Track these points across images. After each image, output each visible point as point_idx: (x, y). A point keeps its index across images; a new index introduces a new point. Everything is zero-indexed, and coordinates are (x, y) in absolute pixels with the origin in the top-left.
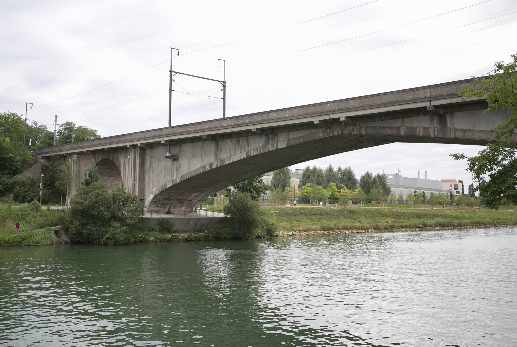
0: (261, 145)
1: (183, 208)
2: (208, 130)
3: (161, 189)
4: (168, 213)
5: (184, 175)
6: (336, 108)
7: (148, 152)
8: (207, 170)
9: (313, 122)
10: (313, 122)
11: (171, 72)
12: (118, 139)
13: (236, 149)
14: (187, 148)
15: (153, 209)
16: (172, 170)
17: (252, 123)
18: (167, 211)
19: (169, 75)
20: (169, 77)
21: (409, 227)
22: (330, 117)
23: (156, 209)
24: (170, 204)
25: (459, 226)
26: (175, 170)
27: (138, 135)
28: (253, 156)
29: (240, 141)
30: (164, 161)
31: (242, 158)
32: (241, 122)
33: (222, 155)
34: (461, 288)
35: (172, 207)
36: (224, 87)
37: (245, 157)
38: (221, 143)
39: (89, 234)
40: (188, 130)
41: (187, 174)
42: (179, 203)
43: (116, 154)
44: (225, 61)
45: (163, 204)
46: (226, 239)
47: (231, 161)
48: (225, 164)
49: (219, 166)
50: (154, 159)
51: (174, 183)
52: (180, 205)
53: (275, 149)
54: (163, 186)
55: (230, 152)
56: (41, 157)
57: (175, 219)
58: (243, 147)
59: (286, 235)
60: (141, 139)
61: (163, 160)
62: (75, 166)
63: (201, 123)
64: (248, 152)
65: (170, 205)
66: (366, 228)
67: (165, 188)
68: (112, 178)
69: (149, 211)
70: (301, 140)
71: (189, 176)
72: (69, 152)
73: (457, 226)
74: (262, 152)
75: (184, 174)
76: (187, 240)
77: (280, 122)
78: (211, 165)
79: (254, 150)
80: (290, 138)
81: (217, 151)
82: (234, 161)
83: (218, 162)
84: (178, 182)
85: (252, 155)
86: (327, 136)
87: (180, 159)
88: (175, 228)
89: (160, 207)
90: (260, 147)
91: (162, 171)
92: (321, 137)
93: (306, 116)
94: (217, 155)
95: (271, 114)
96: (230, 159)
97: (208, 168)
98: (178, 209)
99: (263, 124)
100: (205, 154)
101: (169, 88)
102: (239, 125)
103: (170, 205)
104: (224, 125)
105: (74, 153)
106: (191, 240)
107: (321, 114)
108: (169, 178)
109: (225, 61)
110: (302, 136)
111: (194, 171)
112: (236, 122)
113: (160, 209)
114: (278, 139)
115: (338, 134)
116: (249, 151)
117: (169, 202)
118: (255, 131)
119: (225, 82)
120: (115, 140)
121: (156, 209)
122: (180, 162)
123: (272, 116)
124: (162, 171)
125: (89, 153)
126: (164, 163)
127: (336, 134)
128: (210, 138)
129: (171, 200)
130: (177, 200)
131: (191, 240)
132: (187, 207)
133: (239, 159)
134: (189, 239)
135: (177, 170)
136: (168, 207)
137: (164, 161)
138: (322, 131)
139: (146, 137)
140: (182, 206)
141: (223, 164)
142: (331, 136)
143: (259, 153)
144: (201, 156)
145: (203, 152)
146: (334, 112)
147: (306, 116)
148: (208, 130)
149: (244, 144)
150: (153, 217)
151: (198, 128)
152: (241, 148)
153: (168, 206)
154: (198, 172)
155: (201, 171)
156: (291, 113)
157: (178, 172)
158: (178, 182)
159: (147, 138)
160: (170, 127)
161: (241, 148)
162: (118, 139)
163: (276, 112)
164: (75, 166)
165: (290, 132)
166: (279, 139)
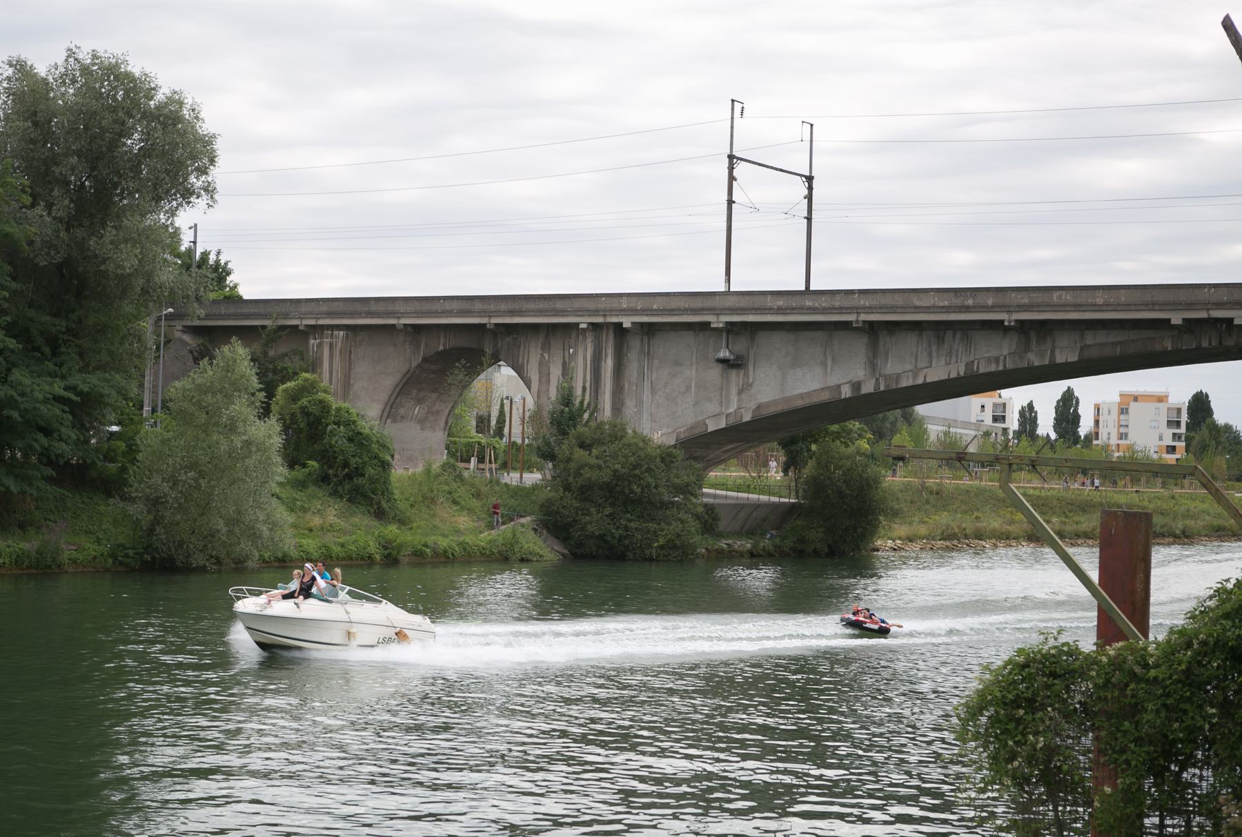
0: (1005, 352)
2: (870, 310)
3: (687, 435)
5: (768, 404)
6: (1225, 298)
7: (635, 344)
8: (843, 397)
9: (1169, 320)
10: (1169, 320)
11: (731, 157)
12: (541, 305)
13: (934, 355)
14: (777, 343)
16: (722, 389)
17: (1005, 306)
20: (727, 171)
21: (1091, 535)
22: (1209, 315)
25: (1187, 537)
26: (734, 391)
27: (624, 300)
28: (982, 374)
29: (943, 339)
30: (694, 367)
31: (953, 375)
32: (970, 302)
33: (889, 365)
36: (810, 188)
37: (962, 373)
38: (885, 340)
39: (621, 539)
40: (802, 303)
41: (775, 402)
43: (508, 339)
44: (812, 125)
47: (920, 381)
48: (900, 386)
49: (882, 388)
50: (656, 361)
51: (731, 421)
53: (1047, 362)
54: (692, 427)
55: (913, 361)
56: (180, 328)
58: (954, 352)
60: (634, 312)
61: (691, 365)
62: (337, 358)
63: (852, 292)
64: (969, 365)
66: (1014, 535)
67: (698, 431)
68: (434, 395)
70: (1118, 350)
71: (785, 407)
72: (321, 322)
73: (1180, 538)
74: (1009, 366)
75: (764, 401)
77: (1081, 313)
78: (856, 386)
79: (989, 360)
80: (1088, 342)
81: (874, 356)
82: (928, 380)
83: (877, 380)
84: (744, 420)
85: (982, 371)
86: (1184, 348)
87: (751, 367)
90: (1005, 357)
91: (688, 389)
92: (1169, 348)
93: (1151, 306)
94: (872, 365)
95: (1055, 295)
96: (915, 376)
97: (846, 392)
99: (1036, 313)
100: (834, 360)
101: (725, 197)
102: (967, 309)
104: (918, 303)
105: (339, 327)
107: (1190, 306)
108: (712, 408)
109: (812, 125)
110: (1120, 343)
111: (801, 396)
112: (958, 302)
114: (1054, 342)
115: (1210, 344)
116: (973, 362)
118: (1013, 324)
119: (810, 179)
120: (531, 306)
122: (751, 372)
123: (1060, 297)
124: (688, 389)
125: (409, 329)
126: (694, 372)
127: (1205, 344)
128: (867, 326)
133: (943, 376)
134: (755, 553)
135: (740, 392)
137: (694, 367)
138: (1173, 336)
139: (655, 307)
141: (894, 386)
142: (1194, 347)
143: (1001, 368)
144: (824, 365)
145: (828, 354)
146: (1219, 305)
147: (1151, 306)
148: (870, 310)
149: (956, 347)
151: (837, 304)
152: (950, 354)
154: (815, 400)
155: (825, 397)
156: (1111, 298)
157: (743, 396)
158: (747, 417)
159: (655, 310)
160: (728, 293)
161: (950, 354)
162: (541, 305)
163: (1071, 292)
164: (337, 358)
165: (1086, 332)
166: (1056, 344)
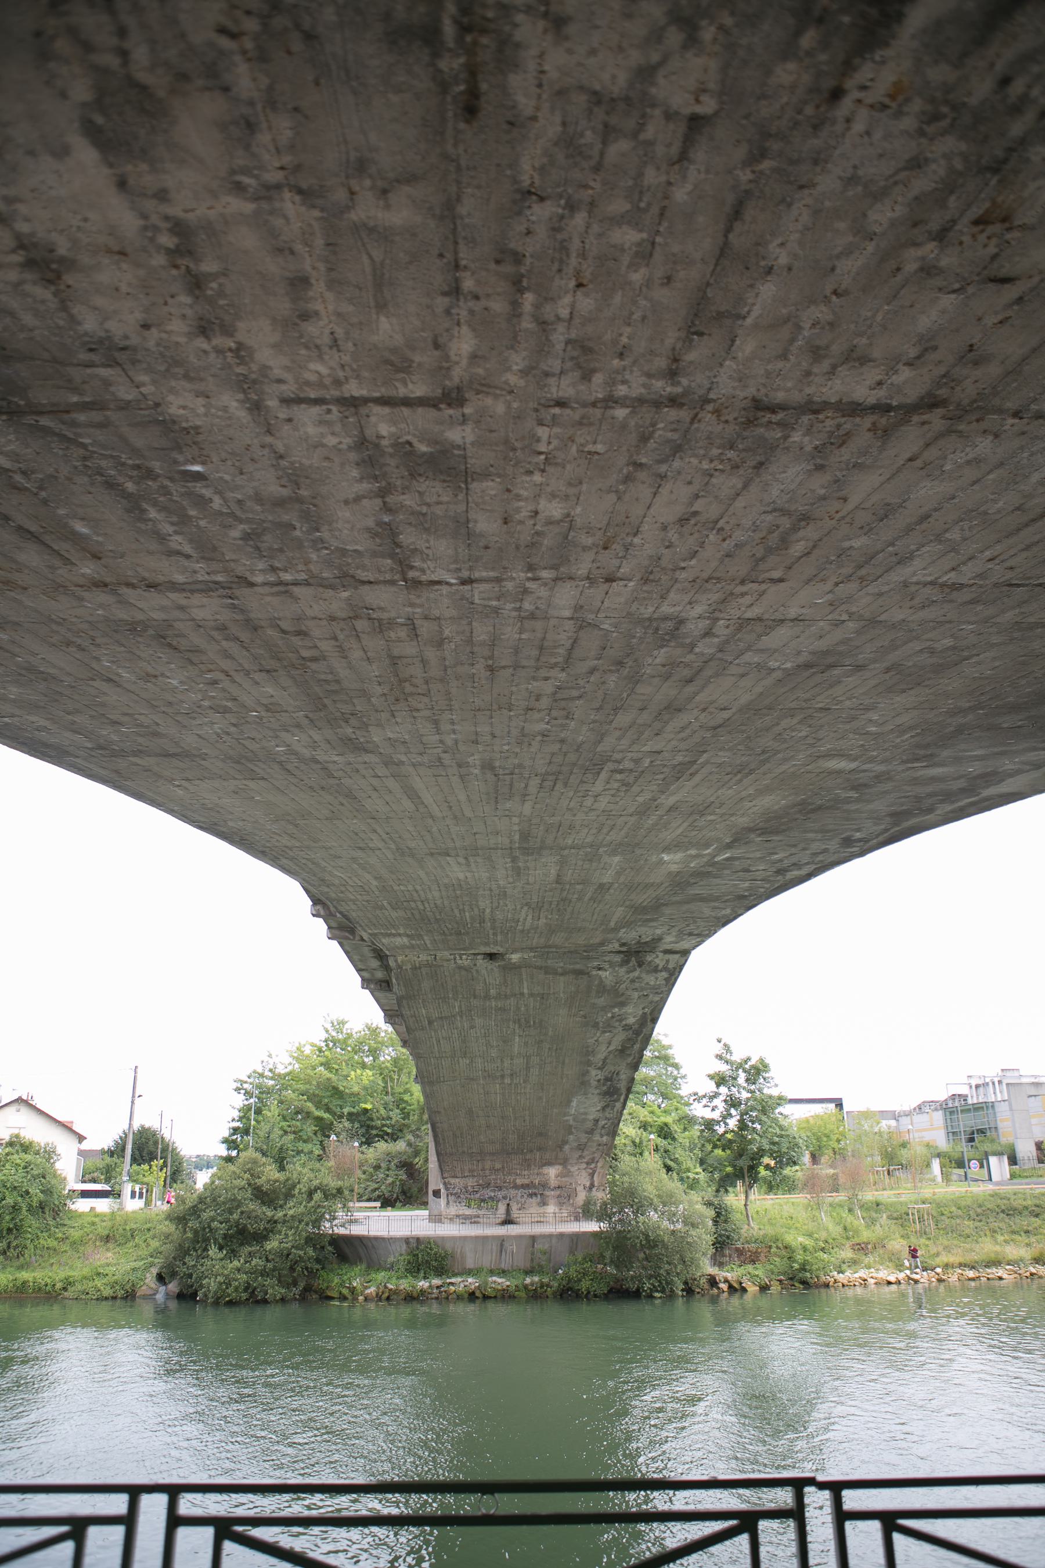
1: (551, 1208)
4: (508, 1221)
15: (461, 1212)
18: (504, 1216)
19: (873, 1109)
23: (468, 1212)
24: (505, 1198)
34: (75, 399)
35: (514, 1207)
42: (531, 1195)
45: (483, 1201)
46: (590, 1297)
48: (386, 1029)
52: (534, 1200)
57: (465, 1239)
59: (873, 1281)
65: (507, 1201)
69: (451, 1219)
76: (472, 1296)
88: (470, 1264)
89: (479, 1208)
98: (532, 1210)
103: (507, 1201)
106: (486, 1298)
113: (480, 1212)
117: (500, 1194)
121: (468, 1212)
129: (500, 1189)
130: (516, 1187)
131: (486, 1298)
132: (561, 1204)
134: (478, 1294)
136: (502, 1209)
140: (544, 1203)
150: (582, 1230)
153: (500, 1204)
